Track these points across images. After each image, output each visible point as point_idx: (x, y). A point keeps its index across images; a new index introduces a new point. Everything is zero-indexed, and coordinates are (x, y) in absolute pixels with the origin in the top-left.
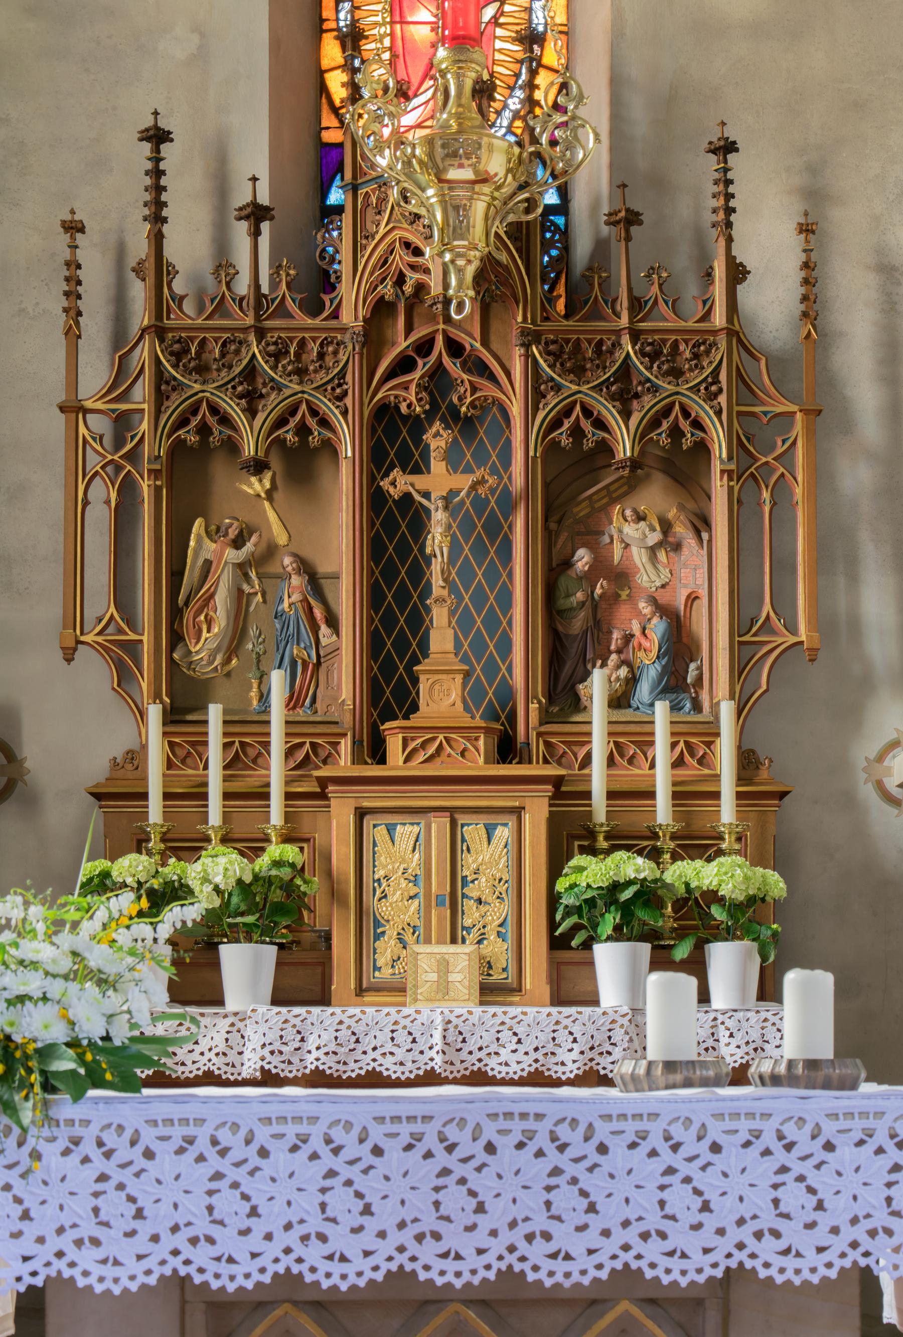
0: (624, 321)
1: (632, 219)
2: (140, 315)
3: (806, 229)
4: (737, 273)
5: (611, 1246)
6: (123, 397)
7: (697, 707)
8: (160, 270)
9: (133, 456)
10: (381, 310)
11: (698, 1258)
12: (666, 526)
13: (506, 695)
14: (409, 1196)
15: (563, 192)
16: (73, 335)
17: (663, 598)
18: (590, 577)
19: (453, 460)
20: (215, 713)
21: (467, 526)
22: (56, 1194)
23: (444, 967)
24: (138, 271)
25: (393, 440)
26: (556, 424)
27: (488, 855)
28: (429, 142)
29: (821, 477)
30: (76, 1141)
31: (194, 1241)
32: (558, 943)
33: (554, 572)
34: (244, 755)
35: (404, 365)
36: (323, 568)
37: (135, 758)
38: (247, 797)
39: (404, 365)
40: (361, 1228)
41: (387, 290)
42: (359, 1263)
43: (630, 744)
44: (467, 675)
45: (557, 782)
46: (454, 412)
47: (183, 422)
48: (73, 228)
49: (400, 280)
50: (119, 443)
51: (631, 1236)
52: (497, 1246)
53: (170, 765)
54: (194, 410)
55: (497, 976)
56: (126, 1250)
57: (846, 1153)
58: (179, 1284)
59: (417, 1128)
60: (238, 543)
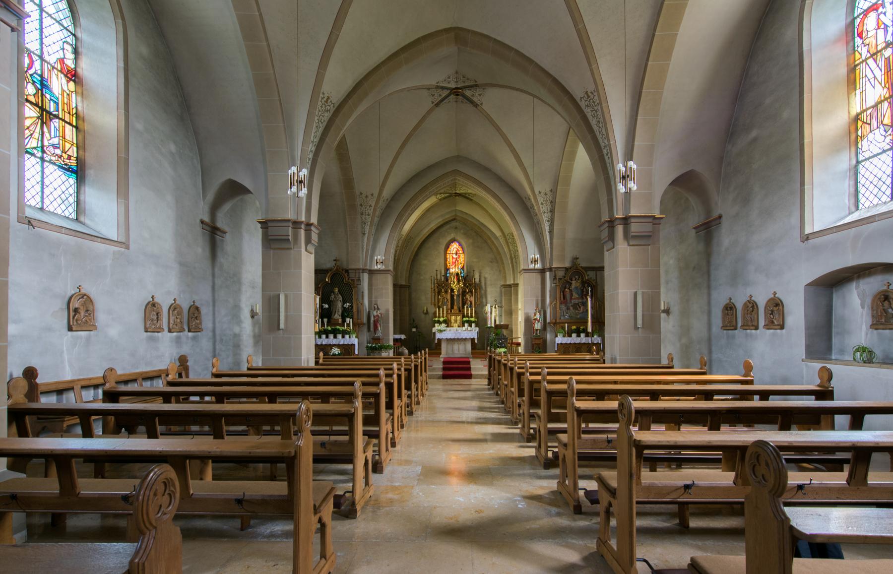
27: (459, 318)
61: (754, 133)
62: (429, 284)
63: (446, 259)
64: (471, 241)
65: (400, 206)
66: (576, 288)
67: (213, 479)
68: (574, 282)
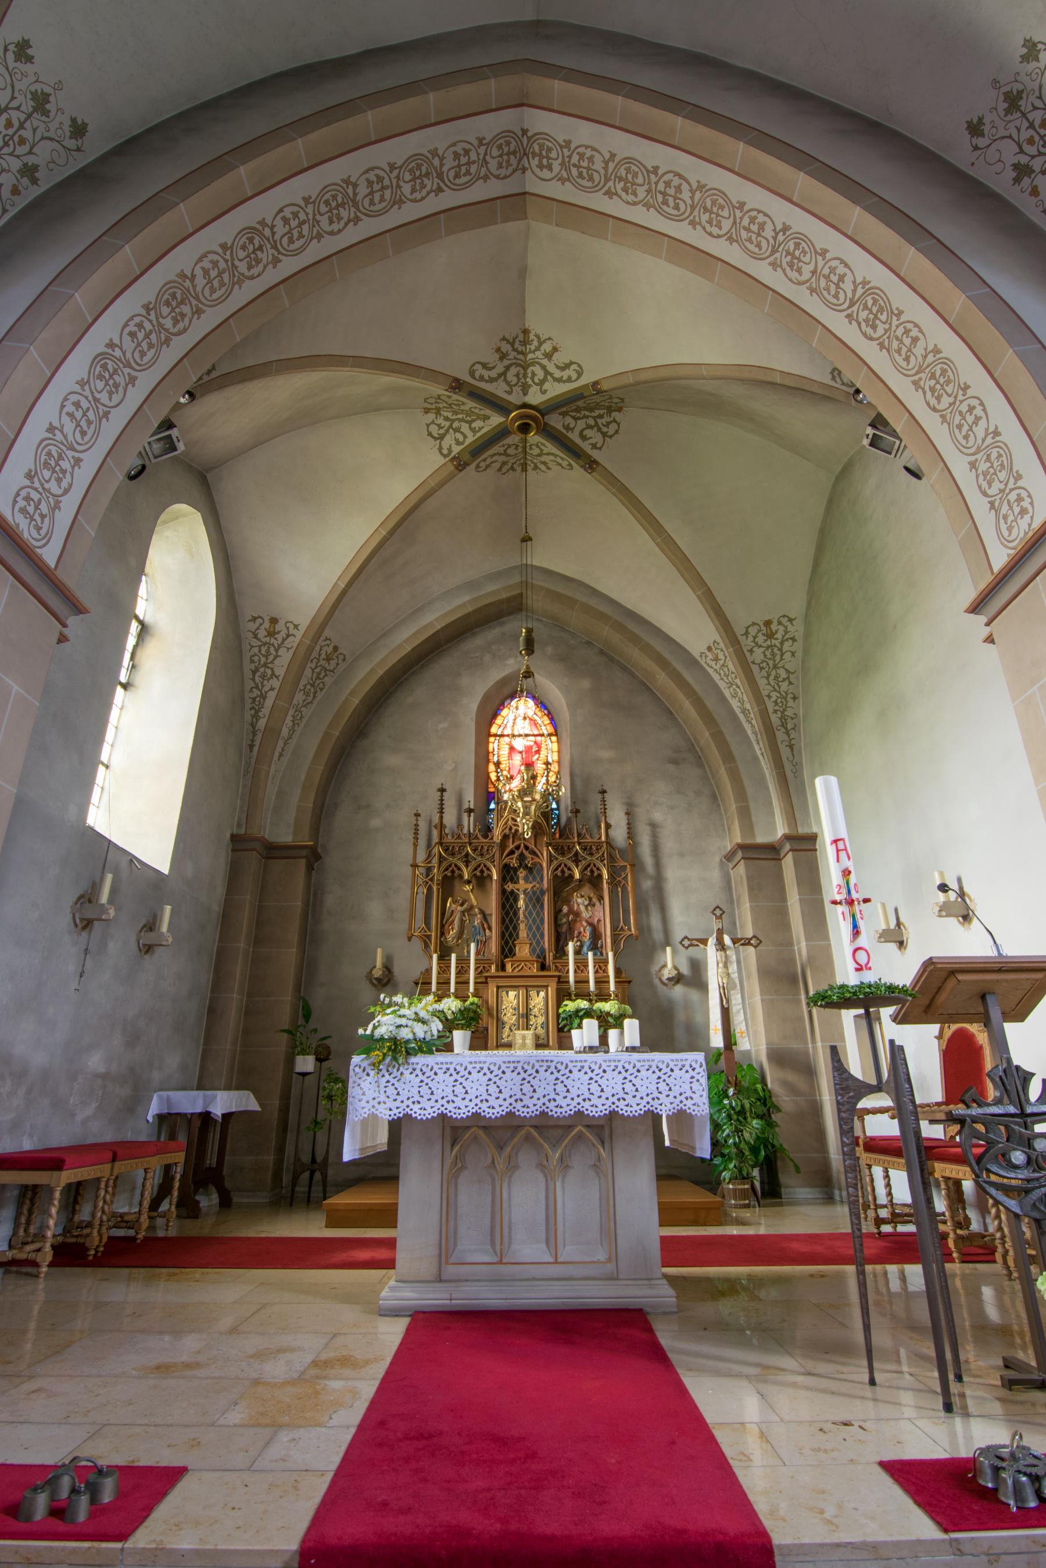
0: (576, 839)
1: (577, 811)
2: (435, 838)
3: (627, 814)
4: (608, 826)
5: (574, 1103)
6: (430, 862)
7: (602, 954)
8: (441, 826)
9: (432, 880)
10: (505, 837)
12: (590, 899)
13: (543, 951)
15: (558, 803)
16: (415, 845)
17: (590, 921)
18: (567, 915)
19: (526, 879)
20: (453, 956)
21: (531, 900)
22: (407, 1087)
23: (524, 1038)
24: (435, 827)
25: (508, 874)
26: (557, 869)
27: (538, 1000)
28: (519, 791)
29: (636, 884)
30: (414, 1070)
32: (560, 1030)
33: (557, 913)
34: (462, 971)
35: (512, 852)
36: (487, 912)
37: (429, 971)
38: (462, 983)
39: (512, 852)
41: (507, 831)
43: (581, 965)
44: (531, 944)
45: (559, 977)
46: (526, 866)
47: (447, 869)
48: (417, 815)
49: (511, 829)
50: (427, 875)
51: (580, 1100)
52: (540, 1103)
53: (439, 973)
54: (450, 866)
55: (541, 1042)
56: (393, 1105)
57: (643, 1073)
58: (443, 1116)
59: (515, 1065)
60: (462, 905)
61: (190, 1345)
62: (405, 851)
63: (483, 756)
64: (586, 684)
65: (161, 174)
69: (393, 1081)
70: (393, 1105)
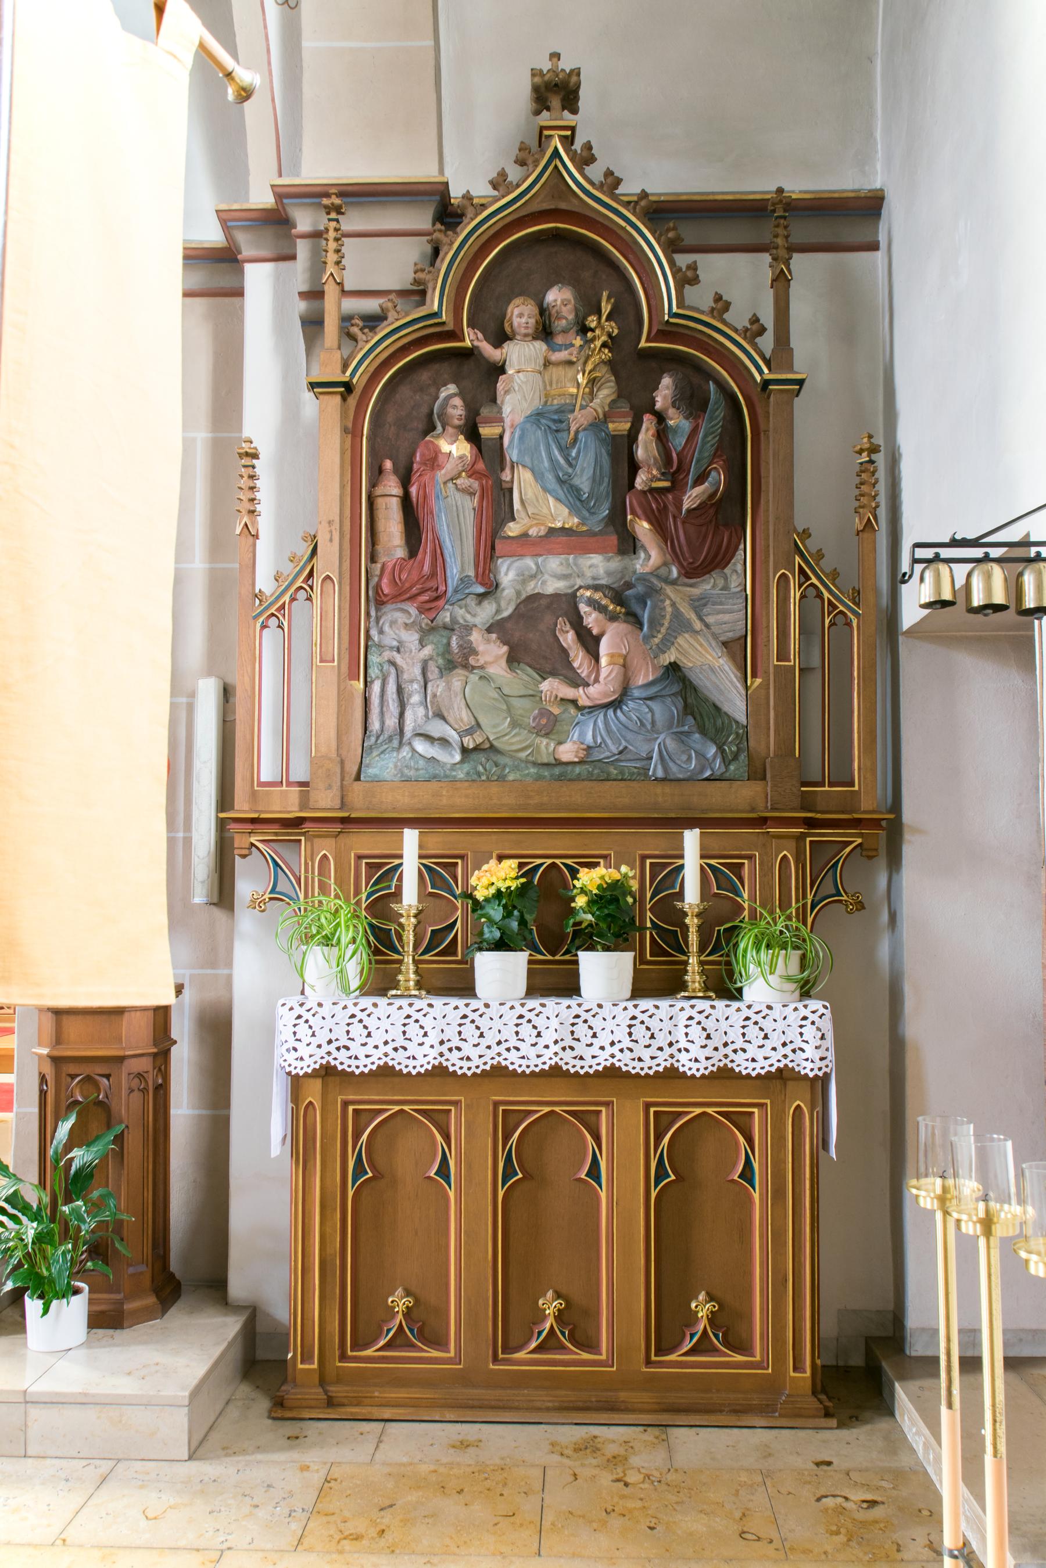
11: (589, 1061)
14: (389, 1028)
31: (396, 1049)
40: (592, 1044)
42: (762, 1062)
56: (532, 1053)
66: (551, 419)
67: (12, 1111)
68: (521, 357)
69: (698, 1017)
70: (701, 1055)
